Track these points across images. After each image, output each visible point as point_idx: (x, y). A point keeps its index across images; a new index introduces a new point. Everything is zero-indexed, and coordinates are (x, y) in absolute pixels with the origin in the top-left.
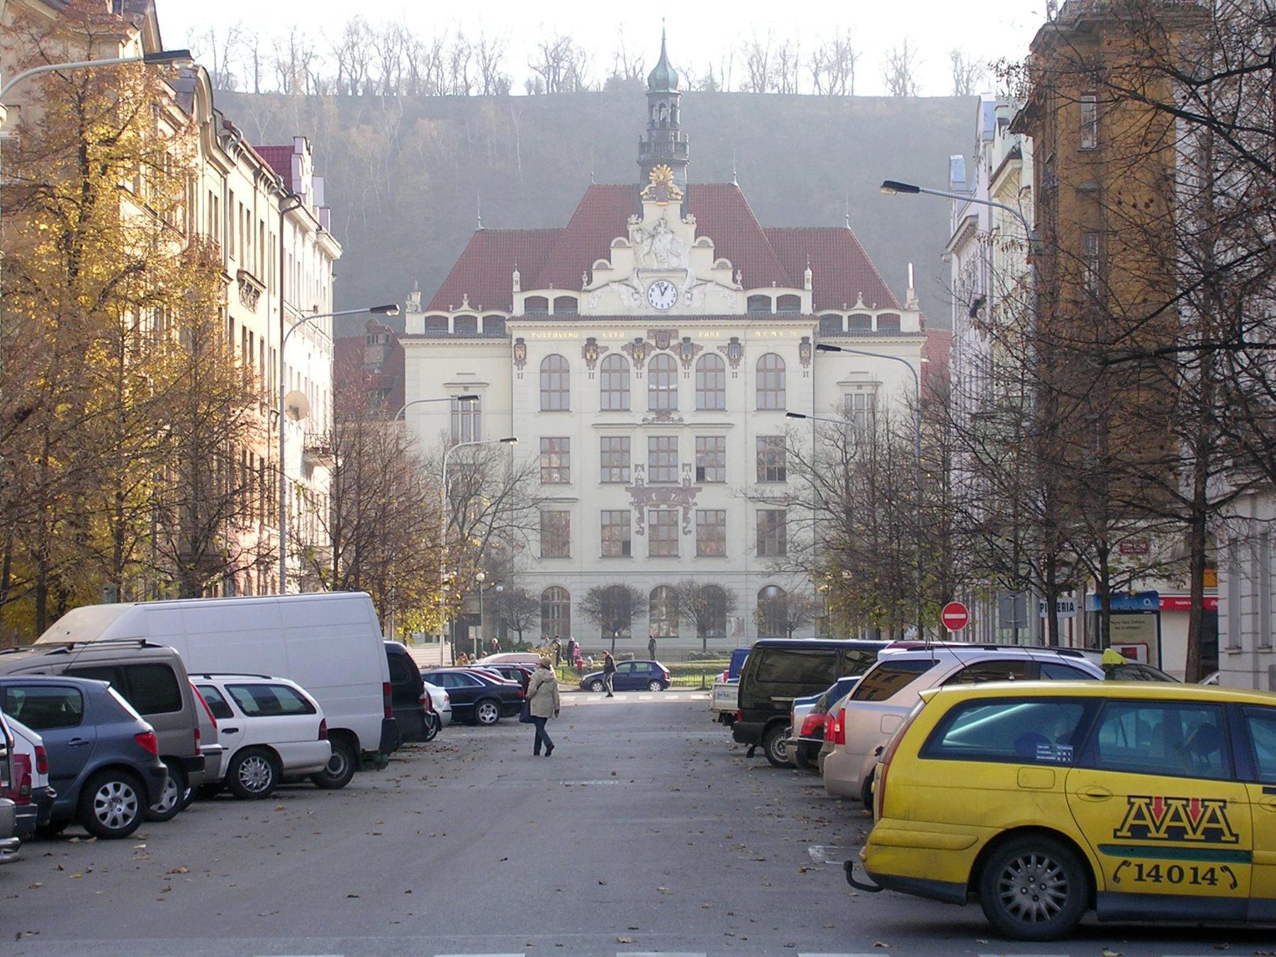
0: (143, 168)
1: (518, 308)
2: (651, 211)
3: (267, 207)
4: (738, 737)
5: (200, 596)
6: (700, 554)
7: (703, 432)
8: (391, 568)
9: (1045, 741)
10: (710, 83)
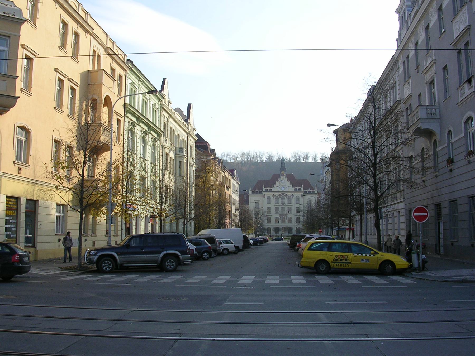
0: (214, 173)
1: (264, 190)
2: (281, 177)
3: (230, 178)
4: (290, 247)
5: (221, 228)
6: (288, 223)
7: (288, 206)
8: (246, 225)
9: (324, 248)
10: (289, 160)
